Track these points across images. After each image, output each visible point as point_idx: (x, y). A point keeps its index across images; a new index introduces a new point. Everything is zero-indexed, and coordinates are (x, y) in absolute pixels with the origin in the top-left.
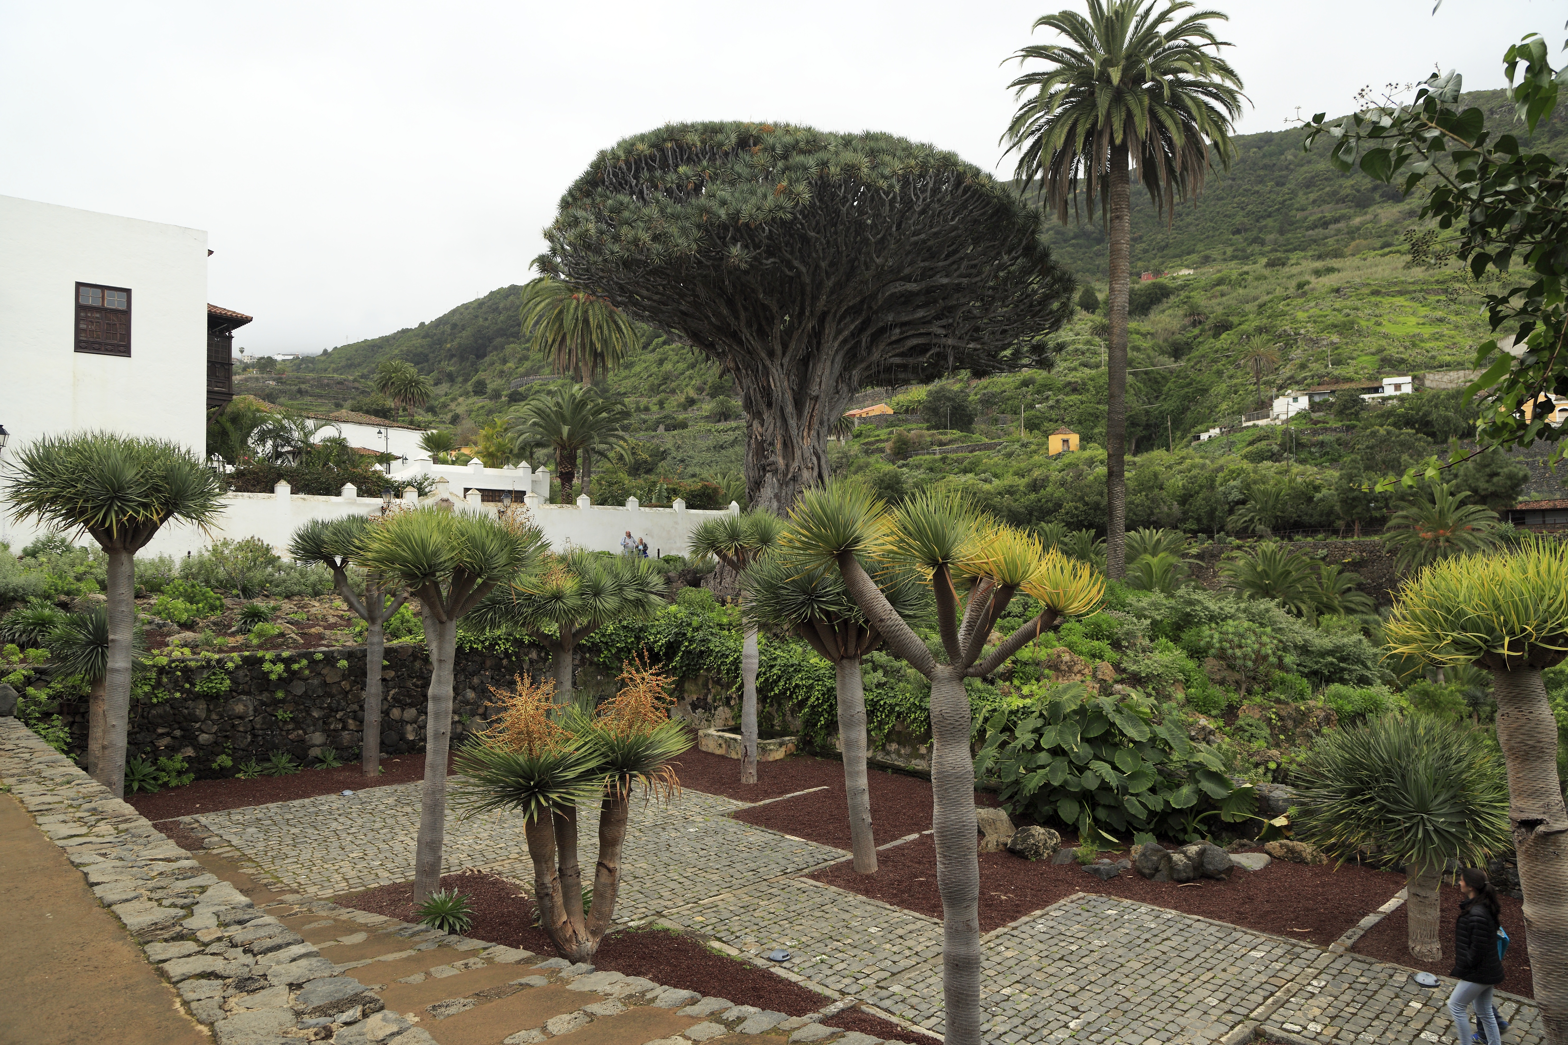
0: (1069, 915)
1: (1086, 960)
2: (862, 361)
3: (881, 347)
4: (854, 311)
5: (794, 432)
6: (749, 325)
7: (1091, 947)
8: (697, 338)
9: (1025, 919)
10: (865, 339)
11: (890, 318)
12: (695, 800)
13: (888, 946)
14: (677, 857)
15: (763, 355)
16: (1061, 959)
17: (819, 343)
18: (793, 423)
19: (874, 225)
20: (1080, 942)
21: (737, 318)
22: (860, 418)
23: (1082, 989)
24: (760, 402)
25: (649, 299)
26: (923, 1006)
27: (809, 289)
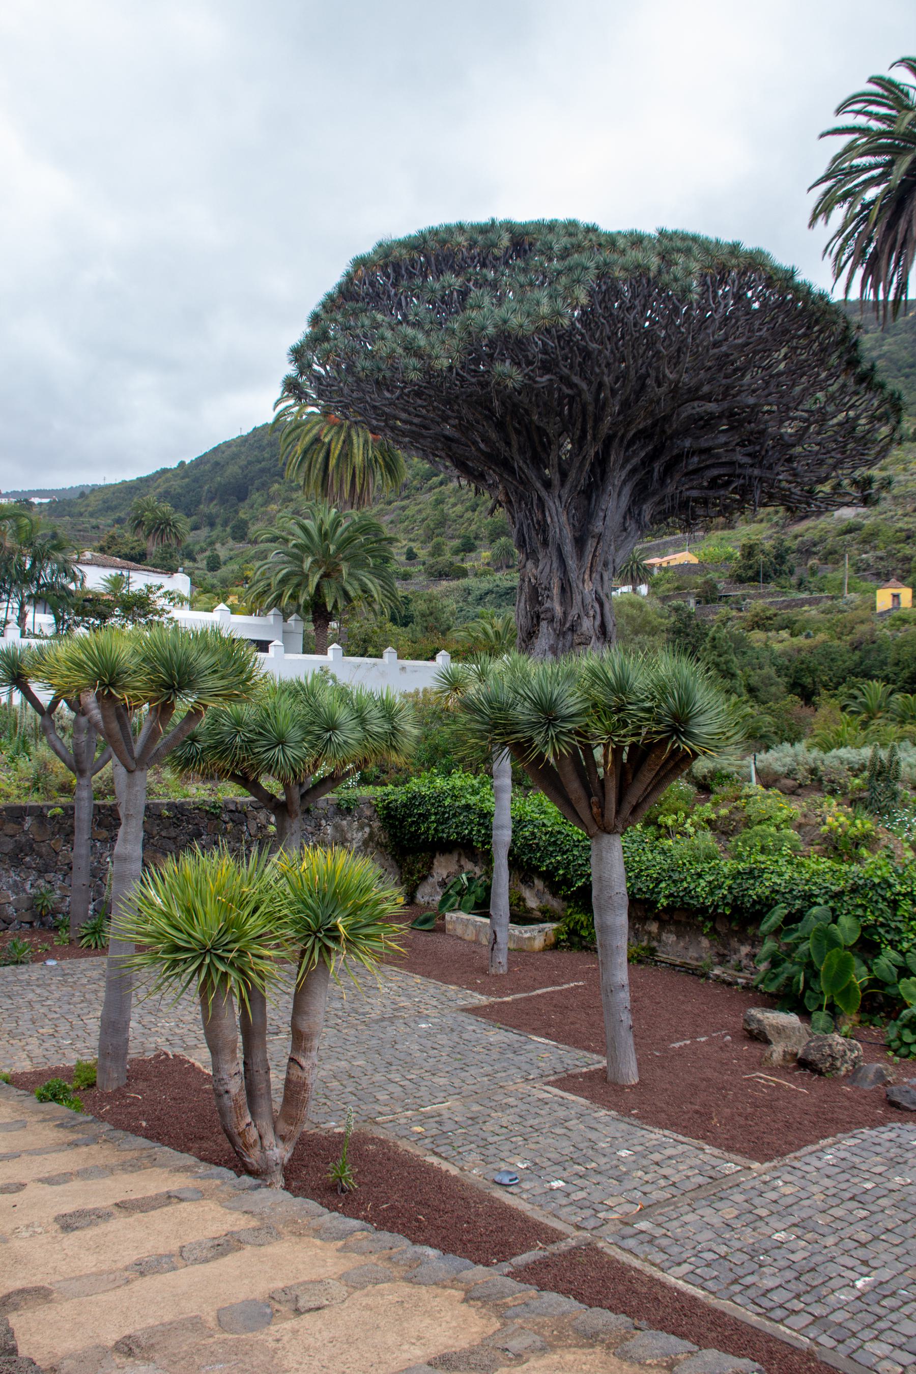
0: (866, 1144)
1: (883, 1202)
2: (654, 494)
3: (677, 477)
4: (644, 435)
5: (573, 576)
6: (522, 451)
7: (891, 1186)
8: (463, 466)
9: (810, 1148)
10: (658, 467)
11: (687, 443)
12: (432, 991)
13: (640, 1173)
14: (402, 1056)
15: (538, 485)
16: (852, 1199)
17: (604, 473)
18: (572, 563)
19: (668, 336)
20: (878, 1179)
21: (508, 444)
22: (660, 568)
23: (876, 1238)
24: (532, 539)
25: (411, 423)
26: (675, 1250)
27: (591, 408)
